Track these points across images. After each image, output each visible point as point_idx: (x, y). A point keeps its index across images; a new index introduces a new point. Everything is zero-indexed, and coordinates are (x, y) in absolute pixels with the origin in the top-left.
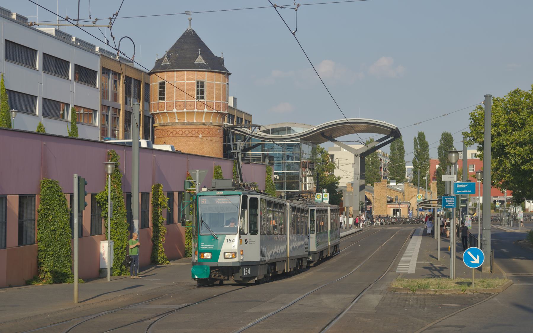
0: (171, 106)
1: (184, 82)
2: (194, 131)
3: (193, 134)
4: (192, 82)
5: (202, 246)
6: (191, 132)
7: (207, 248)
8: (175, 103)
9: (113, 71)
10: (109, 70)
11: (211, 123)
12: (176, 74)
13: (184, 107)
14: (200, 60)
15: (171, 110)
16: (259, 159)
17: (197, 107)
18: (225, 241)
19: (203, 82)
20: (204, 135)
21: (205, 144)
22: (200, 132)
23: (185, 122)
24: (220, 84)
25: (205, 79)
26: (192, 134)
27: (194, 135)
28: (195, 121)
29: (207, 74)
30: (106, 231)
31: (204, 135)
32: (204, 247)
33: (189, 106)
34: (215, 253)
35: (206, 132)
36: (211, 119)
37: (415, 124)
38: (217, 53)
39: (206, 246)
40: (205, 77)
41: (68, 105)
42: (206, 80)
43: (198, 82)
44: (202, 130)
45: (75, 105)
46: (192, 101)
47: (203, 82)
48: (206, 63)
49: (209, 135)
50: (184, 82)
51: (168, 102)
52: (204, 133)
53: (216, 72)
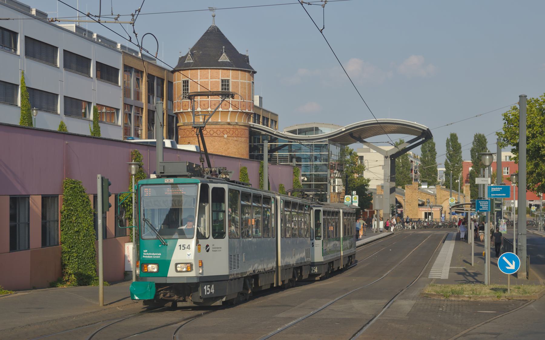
4: (216, 81)
5: (145, 254)
6: (216, 132)
7: (152, 257)
8: (199, 101)
9: (135, 69)
10: (132, 68)
12: (200, 72)
14: (224, 58)
18: (177, 247)
19: (228, 81)
22: (225, 132)
24: (244, 83)
25: (230, 77)
26: (217, 134)
28: (220, 121)
31: (229, 135)
32: (148, 255)
34: (164, 265)
35: (231, 132)
37: (476, 116)
38: (241, 51)
39: (150, 254)
42: (230, 78)
43: (222, 81)
46: (217, 100)
47: (228, 81)
53: (241, 70)
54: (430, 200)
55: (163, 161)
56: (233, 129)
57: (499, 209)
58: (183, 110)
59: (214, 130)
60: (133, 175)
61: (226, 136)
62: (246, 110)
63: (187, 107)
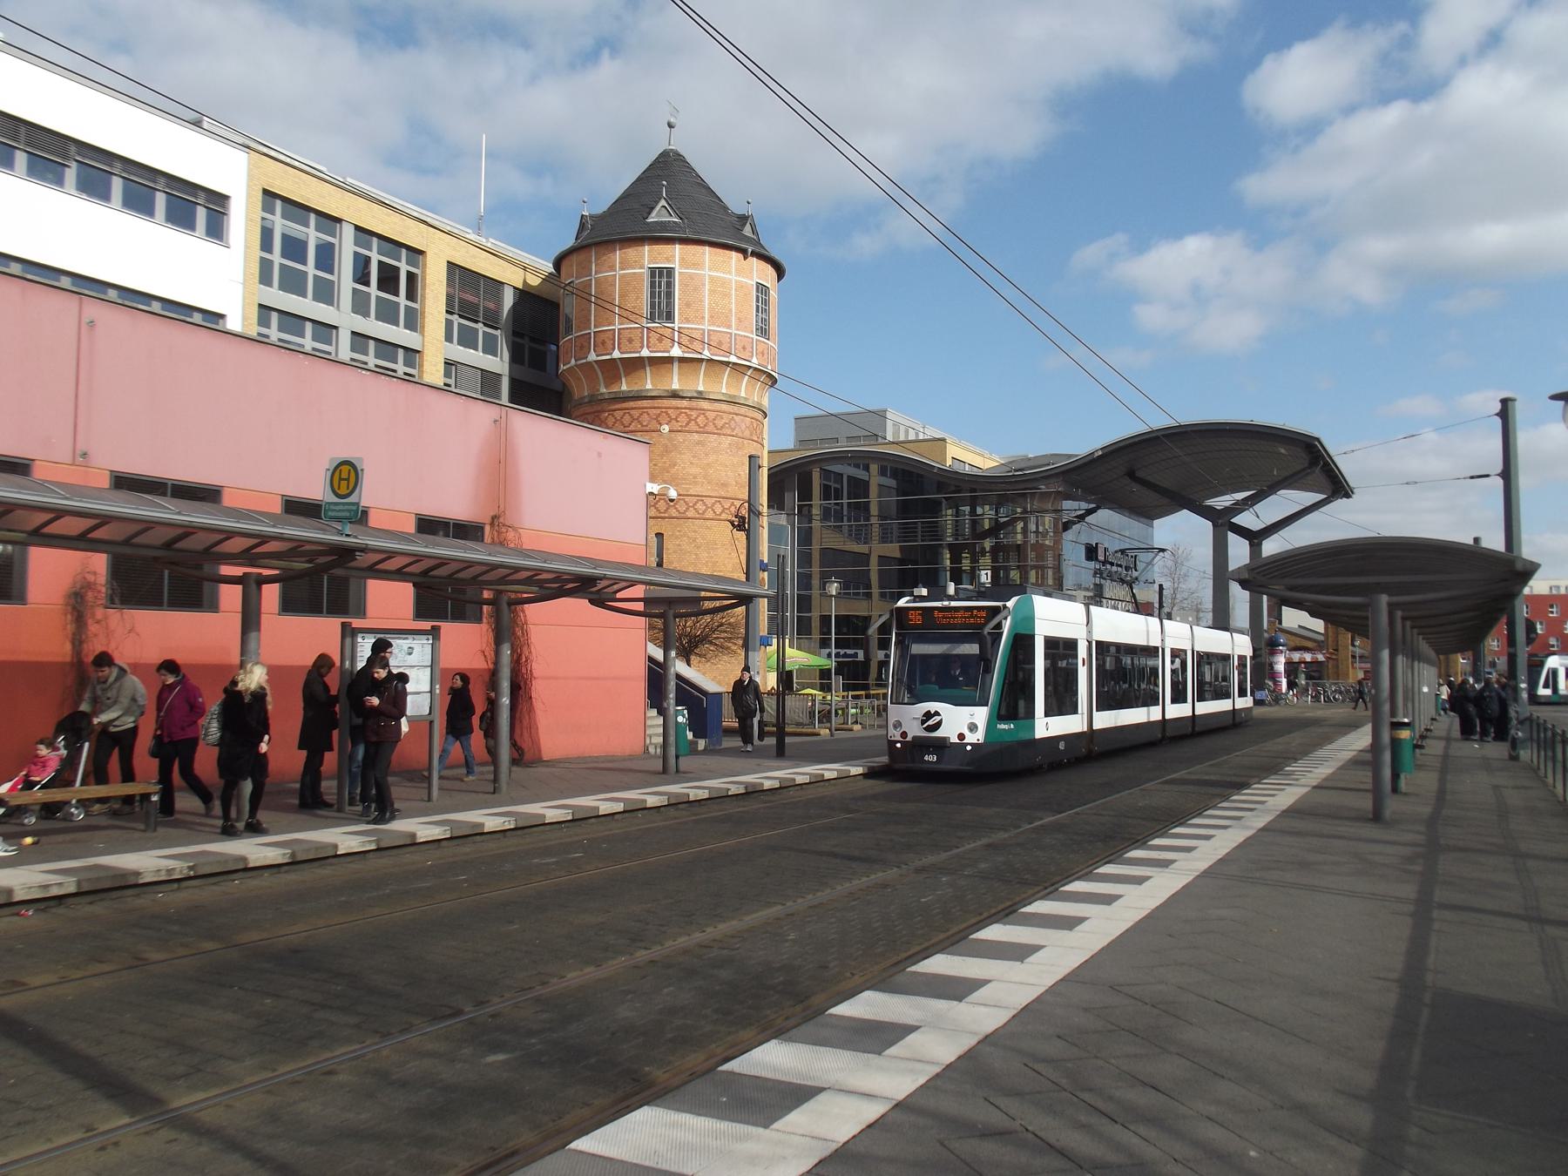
0: (689, 339)
1: (623, 269)
3: (645, 424)
6: (637, 419)
11: (700, 392)
15: (637, 352)
16: (912, 536)
20: (677, 426)
21: (680, 454)
22: (664, 418)
23: (623, 392)
27: (646, 426)
29: (680, 249)
37: (1416, 483)
40: (675, 256)
41: (263, 219)
42: (676, 265)
44: (670, 411)
45: (1299, 626)
48: (681, 219)
49: (692, 426)
50: (614, 273)
51: (714, 331)
54: (1505, 755)
55: (650, 518)
56: (689, 409)
60: (832, 596)
61: (665, 428)
63: (570, 355)
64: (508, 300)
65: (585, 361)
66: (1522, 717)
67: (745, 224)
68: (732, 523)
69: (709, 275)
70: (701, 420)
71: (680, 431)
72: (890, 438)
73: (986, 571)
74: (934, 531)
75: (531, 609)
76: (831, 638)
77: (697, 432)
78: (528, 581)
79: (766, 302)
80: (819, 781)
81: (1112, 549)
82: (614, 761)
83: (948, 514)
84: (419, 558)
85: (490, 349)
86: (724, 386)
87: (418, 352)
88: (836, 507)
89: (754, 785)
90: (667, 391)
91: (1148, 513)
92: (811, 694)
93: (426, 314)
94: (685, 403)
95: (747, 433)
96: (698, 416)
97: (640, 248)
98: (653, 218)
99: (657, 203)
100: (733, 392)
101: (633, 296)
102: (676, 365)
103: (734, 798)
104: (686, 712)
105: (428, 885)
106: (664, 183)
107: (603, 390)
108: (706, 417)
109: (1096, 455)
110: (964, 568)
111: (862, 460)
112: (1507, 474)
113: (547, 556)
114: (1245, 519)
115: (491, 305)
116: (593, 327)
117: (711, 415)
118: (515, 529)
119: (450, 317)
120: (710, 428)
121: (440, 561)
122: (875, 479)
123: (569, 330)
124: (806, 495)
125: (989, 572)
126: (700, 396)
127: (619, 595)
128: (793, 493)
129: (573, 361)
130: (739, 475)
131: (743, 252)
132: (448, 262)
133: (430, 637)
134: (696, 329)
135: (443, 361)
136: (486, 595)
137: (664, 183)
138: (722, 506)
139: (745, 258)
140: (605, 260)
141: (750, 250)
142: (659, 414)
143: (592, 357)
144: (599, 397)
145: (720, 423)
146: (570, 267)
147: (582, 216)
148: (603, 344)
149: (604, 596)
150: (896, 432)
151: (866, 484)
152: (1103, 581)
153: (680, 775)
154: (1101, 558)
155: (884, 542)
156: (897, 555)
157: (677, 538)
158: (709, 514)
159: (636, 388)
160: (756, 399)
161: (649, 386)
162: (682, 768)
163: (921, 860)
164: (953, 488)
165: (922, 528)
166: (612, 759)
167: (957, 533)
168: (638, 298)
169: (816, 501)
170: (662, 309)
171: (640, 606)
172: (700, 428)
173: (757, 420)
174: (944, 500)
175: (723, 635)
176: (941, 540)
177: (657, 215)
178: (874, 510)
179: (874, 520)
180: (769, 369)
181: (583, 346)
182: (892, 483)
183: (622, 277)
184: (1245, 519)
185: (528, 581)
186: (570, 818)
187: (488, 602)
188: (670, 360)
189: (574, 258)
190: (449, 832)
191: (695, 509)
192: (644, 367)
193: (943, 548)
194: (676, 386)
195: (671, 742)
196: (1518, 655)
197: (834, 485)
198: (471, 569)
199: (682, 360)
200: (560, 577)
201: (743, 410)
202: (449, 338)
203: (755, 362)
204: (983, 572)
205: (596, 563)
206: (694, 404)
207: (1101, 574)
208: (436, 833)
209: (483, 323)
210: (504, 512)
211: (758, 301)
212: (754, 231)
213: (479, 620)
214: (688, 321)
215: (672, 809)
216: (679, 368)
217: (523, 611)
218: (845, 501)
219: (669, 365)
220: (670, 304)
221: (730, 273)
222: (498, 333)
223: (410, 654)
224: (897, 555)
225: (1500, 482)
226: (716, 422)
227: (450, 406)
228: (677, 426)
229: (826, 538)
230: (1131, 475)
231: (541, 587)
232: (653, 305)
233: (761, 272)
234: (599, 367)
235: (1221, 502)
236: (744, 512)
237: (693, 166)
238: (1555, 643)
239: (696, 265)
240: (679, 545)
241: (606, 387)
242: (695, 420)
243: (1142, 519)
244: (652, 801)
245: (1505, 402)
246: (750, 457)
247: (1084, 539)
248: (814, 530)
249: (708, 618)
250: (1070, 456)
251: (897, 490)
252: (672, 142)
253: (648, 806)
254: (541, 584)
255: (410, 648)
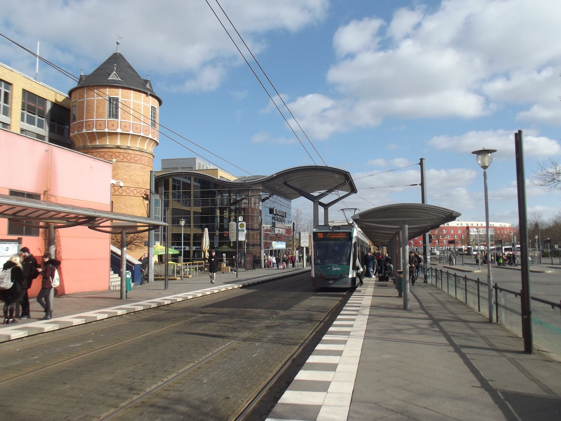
2: (106, 155)
8: (95, 121)
11: (128, 147)
12: (109, 91)
13: (93, 126)
17: (108, 126)
20: (119, 159)
22: (114, 156)
23: (97, 145)
25: (119, 96)
30: (465, 304)
33: (112, 125)
36: (151, 147)
37: (373, 188)
42: (120, 97)
44: (116, 154)
48: (122, 79)
52: (119, 158)
57: (516, 241)
58: (77, 132)
59: (127, 161)
60: (182, 226)
61: (114, 160)
62: (155, 138)
64: (49, 107)
65: (81, 132)
66: (428, 268)
67: (147, 84)
68: (143, 197)
69: (133, 102)
70: (129, 157)
71: (120, 161)
72: (197, 169)
73: (241, 217)
74: (214, 202)
75: (61, 231)
76: (182, 242)
77: (127, 162)
78: (62, 218)
79: (155, 114)
80: (186, 300)
81: (278, 210)
82: (97, 294)
83: (218, 197)
84: (14, 206)
85: (40, 125)
86: (138, 145)
87: (9, 125)
88: (178, 193)
89: (160, 303)
90: (115, 146)
91: (289, 197)
92: (173, 264)
93: (13, 110)
94: (122, 151)
95: (147, 163)
96: (128, 156)
97: (105, 89)
98: (110, 78)
99: (112, 72)
100: (142, 147)
101: (101, 108)
102: (119, 136)
103: (153, 309)
104: (130, 273)
105: (19, 363)
106: (115, 65)
107: (89, 144)
108: (131, 156)
109: (274, 176)
110: (224, 216)
111: (188, 175)
112: (422, 184)
113: (74, 207)
114: (323, 200)
115: (41, 108)
116: (85, 119)
117: (133, 156)
118: (55, 197)
119: (23, 111)
120: (132, 161)
121: (24, 208)
122: (193, 183)
123: (74, 120)
124: (167, 188)
125: (242, 217)
126: (129, 148)
127: (101, 225)
128: (162, 188)
129: (76, 132)
130: (144, 179)
131: (146, 94)
132: (23, 89)
133: (17, 243)
134: (127, 122)
135: (20, 129)
136: (41, 224)
137: (115, 65)
138: (137, 191)
139: (147, 96)
140: (90, 93)
141: (149, 93)
142: (112, 155)
143: (84, 131)
144: (87, 147)
145: (136, 159)
146: (75, 95)
147: (81, 75)
148: (89, 126)
149: (95, 225)
150: (200, 166)
151: (190, 185)
152: (275, 221)
153: (128, 300)
154: (275, 213)
155: (196, 206)
156: (200, 211)
157: (118, 203)
158: (132, 194)
159: (102, 144)
160: (150, 150)
161: (108, 143)
162: (128, 296)
163: (242, 335)
164: (220, 187)
165: (211, 201)
166: (96, 293)
167: (222, 203)
168: (104, 108)
169: (171, 191)
170: (114, 114)
171: (108, 229)
172: (129, 160)
173: (150, 158)
174: (217, 191)
175: (139, 241)
176: (216, 206)
177: (112, 77)
178: (192, 194)
179: (192, 198)
180: (156, 139)
181: (81, 126)
182: (198, 185)
183: (97, 100)
184: (323, 200)
185: (62, 218)
186: (84, 322)
187: (42, 227)
188: (116, 134)
189: (77, 91)
190: (27, 333)
191: (126, 192)
192: (146, 141)
193: (217, 209)
194: (119, 143)
195: (124, 286)
196: (427, 246)
197: (177, 185)
198: (39, 212)
199: (121, 134)
200: (77, 217)
201: (145, 154)
202: (22, 120)
203: (150, 136)
204: (240, 217)
205: (96, 211)
206: (126, 151)
207: (274, 218)
208: (21, 334)
209: (38, 115)
210: (50, 189)
211: (152, 113)
212: (150, 86)
213: (37, 235)
214: (124, 119)
215: (128, 315)
216: (120, 137)
217: (58, 231)
218: (181, 191)
219: (116, 136)
220: (117, 112)
221: (141, 101)
222: (44, 119)
223: (7, 250)
224: (200, 211)
225: (420, 186)
226: (135, 158)
227: (26, 143)
228: (119, 159)
229: (174, 204)
230: (285, 183)
231: (68, 221)
232: (110, 112)
233: (152, 102)
234: (88, 135)
235: (316, 194)
236: (148, 194)
237: (126, 59)
238: (412, 242)
239: (127, 97)
240: (119, 206)
241: (90, 143)
242: (126, 157)
243: (288, 200)
244: (120, 312)
245: (421, 160)
246: (151, 171)
247: (269, 206)
248: (170, 202)
249: (132, 235)
250: (264, 176)
251: (200, 187)
252: (118, 50)
253: (118, 315)
254: (68, 220)
255: (7, 248)
